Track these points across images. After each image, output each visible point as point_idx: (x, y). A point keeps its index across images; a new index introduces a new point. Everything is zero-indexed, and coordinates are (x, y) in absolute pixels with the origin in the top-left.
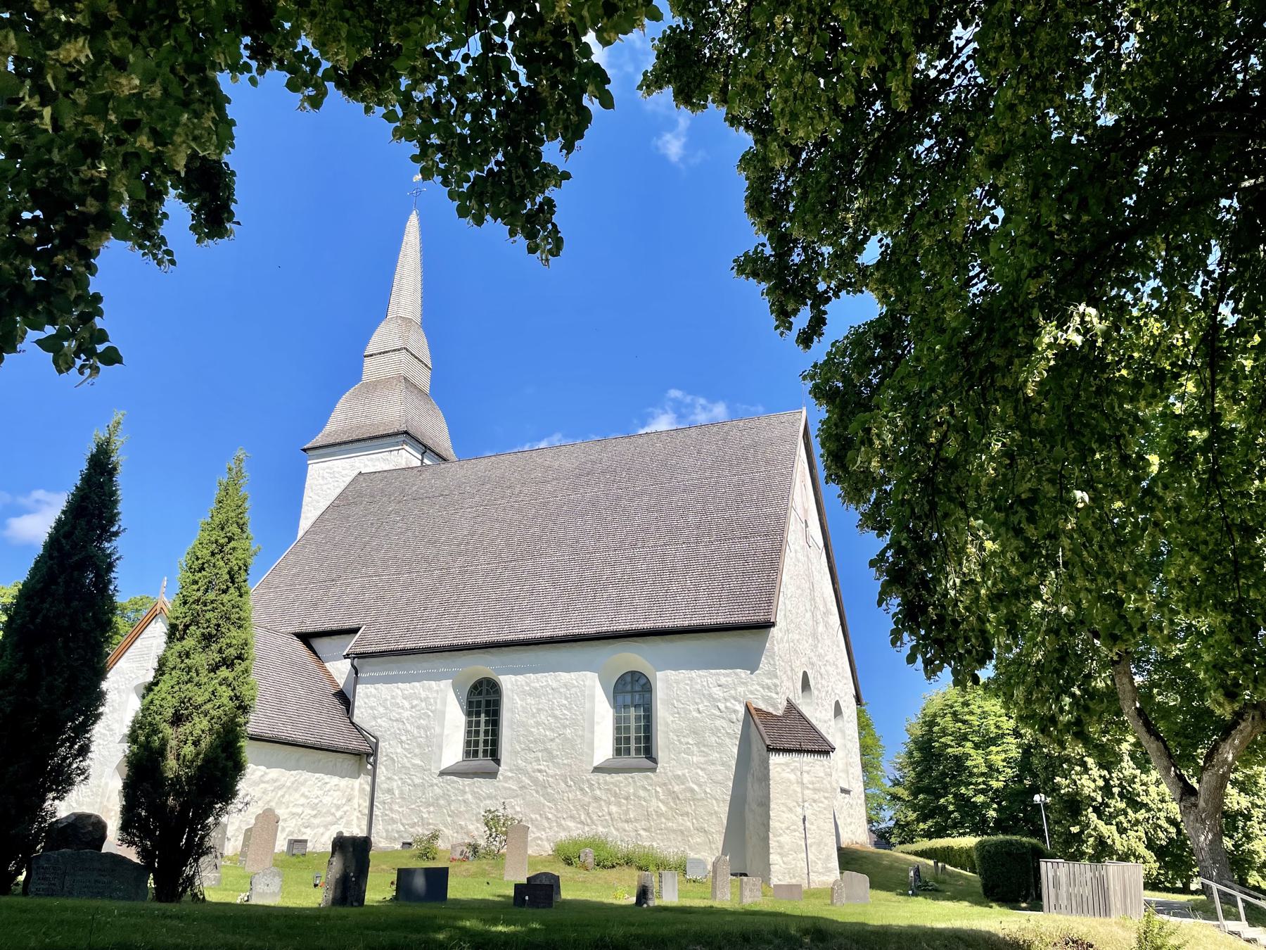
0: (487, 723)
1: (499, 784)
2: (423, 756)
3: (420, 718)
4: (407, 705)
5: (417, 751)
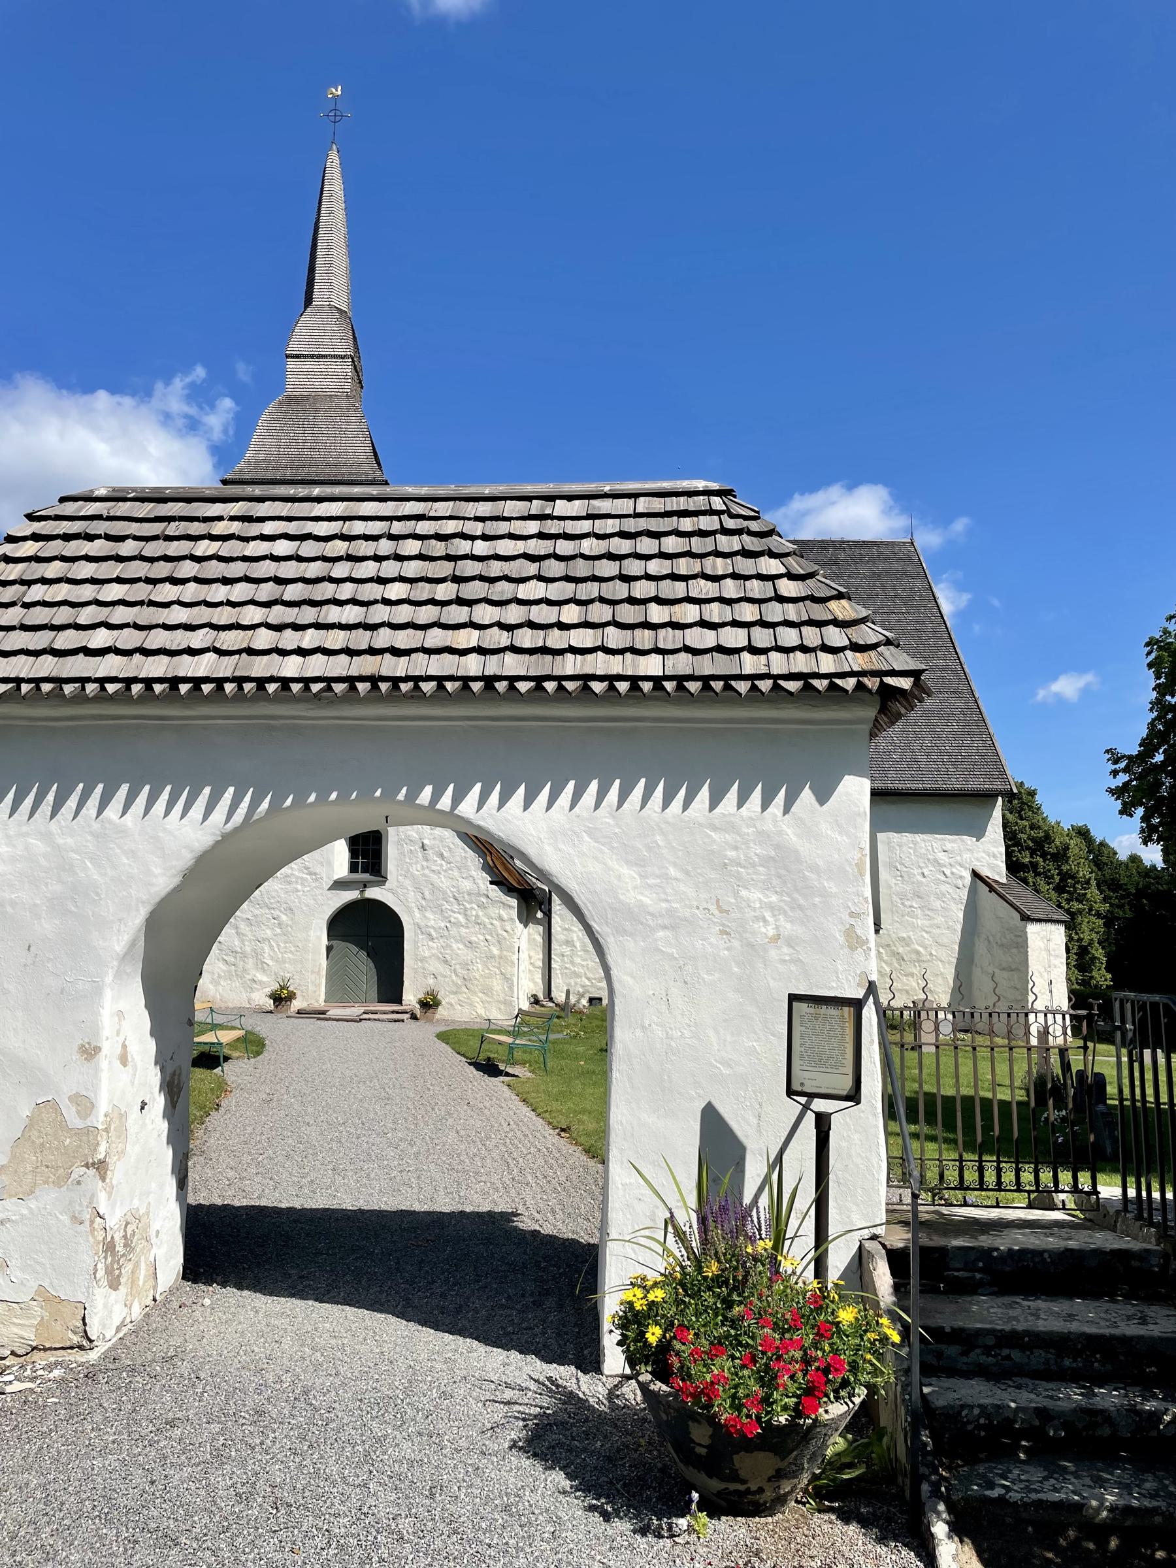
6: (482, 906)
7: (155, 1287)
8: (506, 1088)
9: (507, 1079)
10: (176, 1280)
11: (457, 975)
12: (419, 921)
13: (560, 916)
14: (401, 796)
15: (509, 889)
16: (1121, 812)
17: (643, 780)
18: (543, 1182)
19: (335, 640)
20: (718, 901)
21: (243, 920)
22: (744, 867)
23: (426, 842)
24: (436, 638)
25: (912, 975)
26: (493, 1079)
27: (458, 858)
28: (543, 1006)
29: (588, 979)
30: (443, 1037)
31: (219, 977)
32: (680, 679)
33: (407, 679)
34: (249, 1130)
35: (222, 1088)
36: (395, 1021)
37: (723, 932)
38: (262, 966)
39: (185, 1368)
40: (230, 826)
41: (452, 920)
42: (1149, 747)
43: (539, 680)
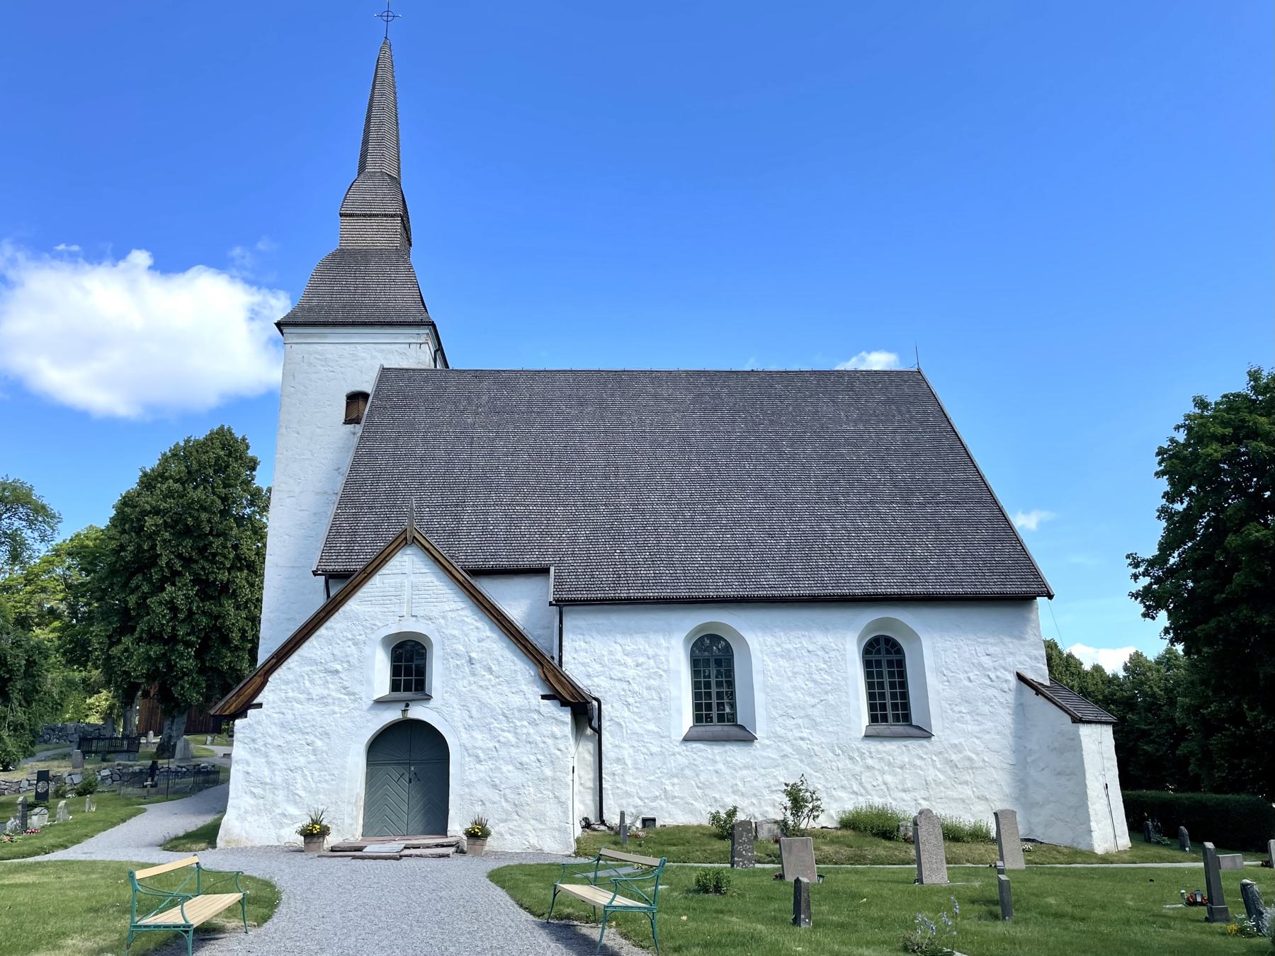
6: (533, 723)
11: (507, 801)
16: (1145, 615)
23: (473, 655)
25: (966, 783)
28: (595, 830)
29: (640, 798)
30: (497, 877)
38: (293, 798)
41: (502, 739)
42: (1166, 547)
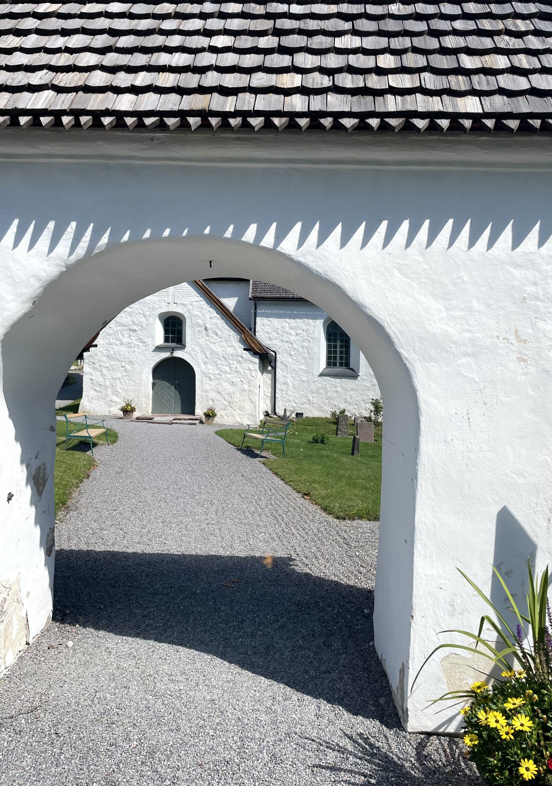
0: (341, 347)
1: (359, 383)
2: (307, 364)
3: (303, 341)
4: (293, 332)
5: (302, 361)
6: (239, 362)
7: (27, 635)
8: (262, 465)
9: (262, 459)
10: (47, 623)
11: (225, 400)
12: (204, 370)
13: (281, 369)
14: (228, 234)
15: (255, 353)
17: (451, 221)
18: (303, 533)
19: (167, 80)
20: (516, 331)
21: (105, 367)
22: (542, 301)
23: (207, 326)
24: (260, 80)
26: (253, 459)
27: (226, 336)
28: (271, 417)
29: (296, 403)
30: (220, 433)
31: (92, 398)
32: (499, 117)
33: (236, 114)
34: (107, 492)
35: (92, 464)
36: (192, 424)
37: (521, 360)
39: (46, 721)
40: (73, 258)
41: (223, 370)
43: (362, 116)
